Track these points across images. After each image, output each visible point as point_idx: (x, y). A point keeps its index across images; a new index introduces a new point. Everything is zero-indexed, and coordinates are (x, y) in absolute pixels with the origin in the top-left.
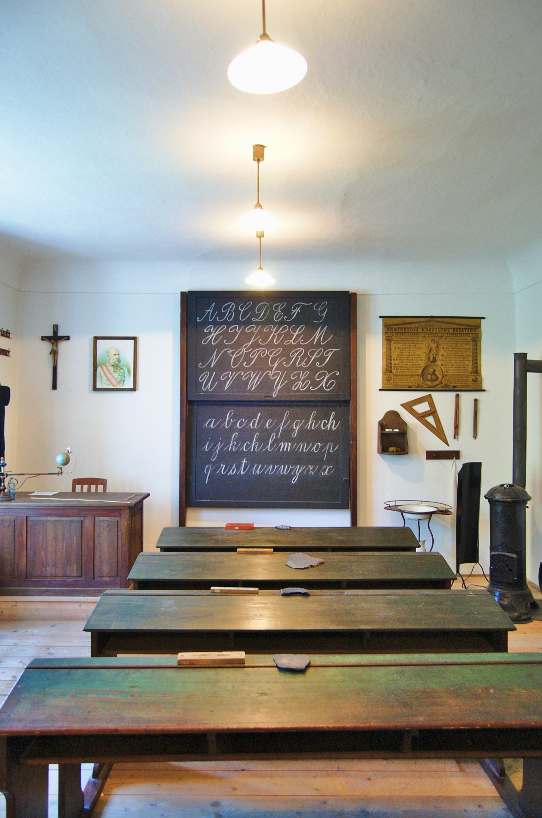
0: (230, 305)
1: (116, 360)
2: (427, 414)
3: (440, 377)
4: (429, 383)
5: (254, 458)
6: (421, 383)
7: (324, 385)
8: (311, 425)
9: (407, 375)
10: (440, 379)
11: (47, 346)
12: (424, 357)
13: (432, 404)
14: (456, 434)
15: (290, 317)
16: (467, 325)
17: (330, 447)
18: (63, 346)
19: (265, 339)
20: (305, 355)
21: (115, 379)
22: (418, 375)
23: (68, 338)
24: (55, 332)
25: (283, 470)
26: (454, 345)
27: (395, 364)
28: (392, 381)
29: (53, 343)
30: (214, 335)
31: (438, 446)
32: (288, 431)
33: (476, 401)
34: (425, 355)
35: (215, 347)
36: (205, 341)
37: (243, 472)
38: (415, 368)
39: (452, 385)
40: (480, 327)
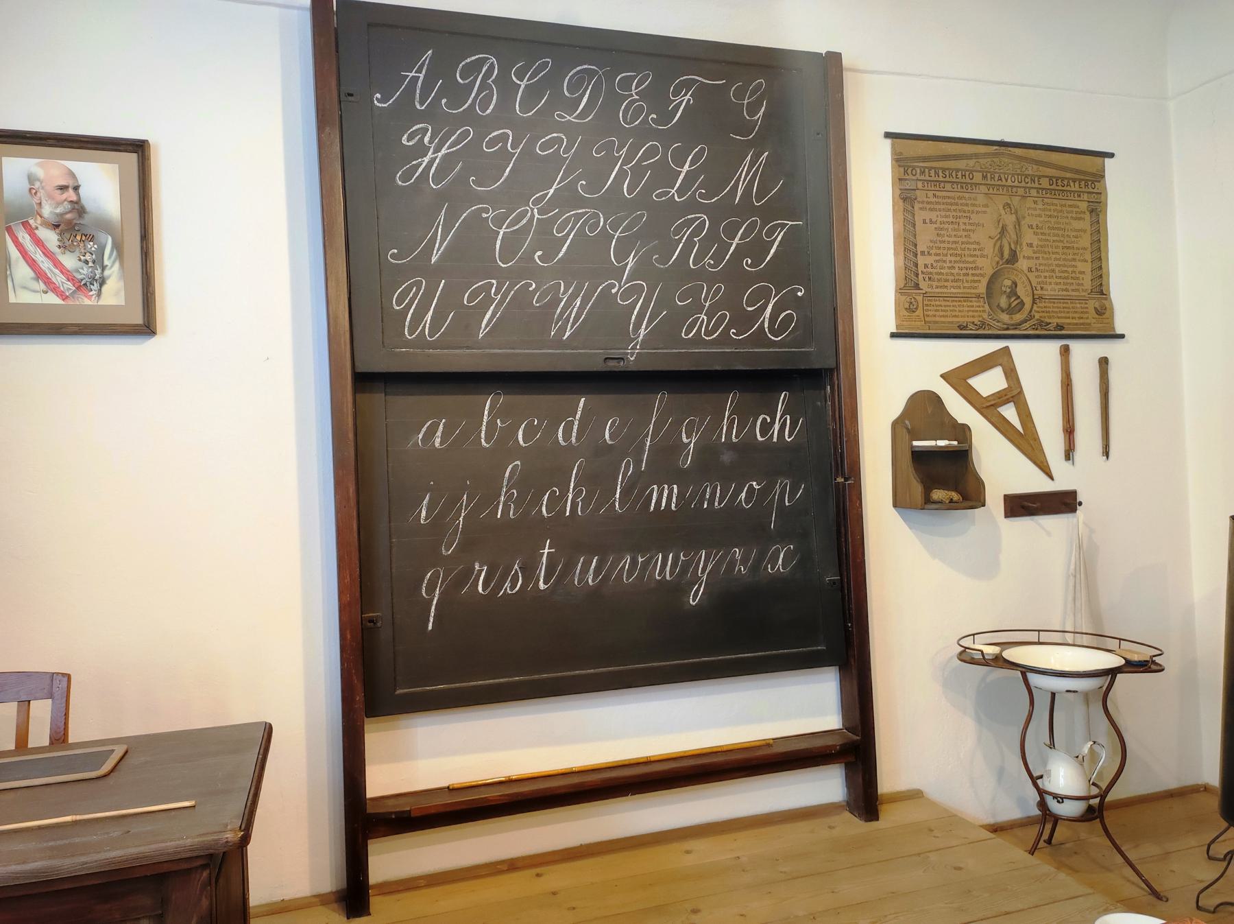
0: (481, 62)
1: (67, 206)
2: (1002, 398)
3: (1028, 301)
4: (1005, 317)
5: (576, 539)
6: (985, 316)
7: (766, 325)
8: (729, 431)
9: (953, 297)
10: (1027, 306)
12: (989, 248)
13: (1011, 373)
14: (1069, 454)
15: (666, 116)
16: (1077, 172)
17: (786, 494)
19: (596, 181)
20: (713, 236)
21: (63, 270)
22: (978, 297)
25: (663, 567)
26: (1053, 220)
27: (926, 266)
28: (919, 312)
30: (432, 159)
31: (1031, 481)
32: (668, 450)
33: (1104, 362)
34: (992, 242)
35: (441, 197)
36: (405, 178)
37: (545, 583)
38: (970, 278)
39: (1055, 321)
40: (1103, 177)
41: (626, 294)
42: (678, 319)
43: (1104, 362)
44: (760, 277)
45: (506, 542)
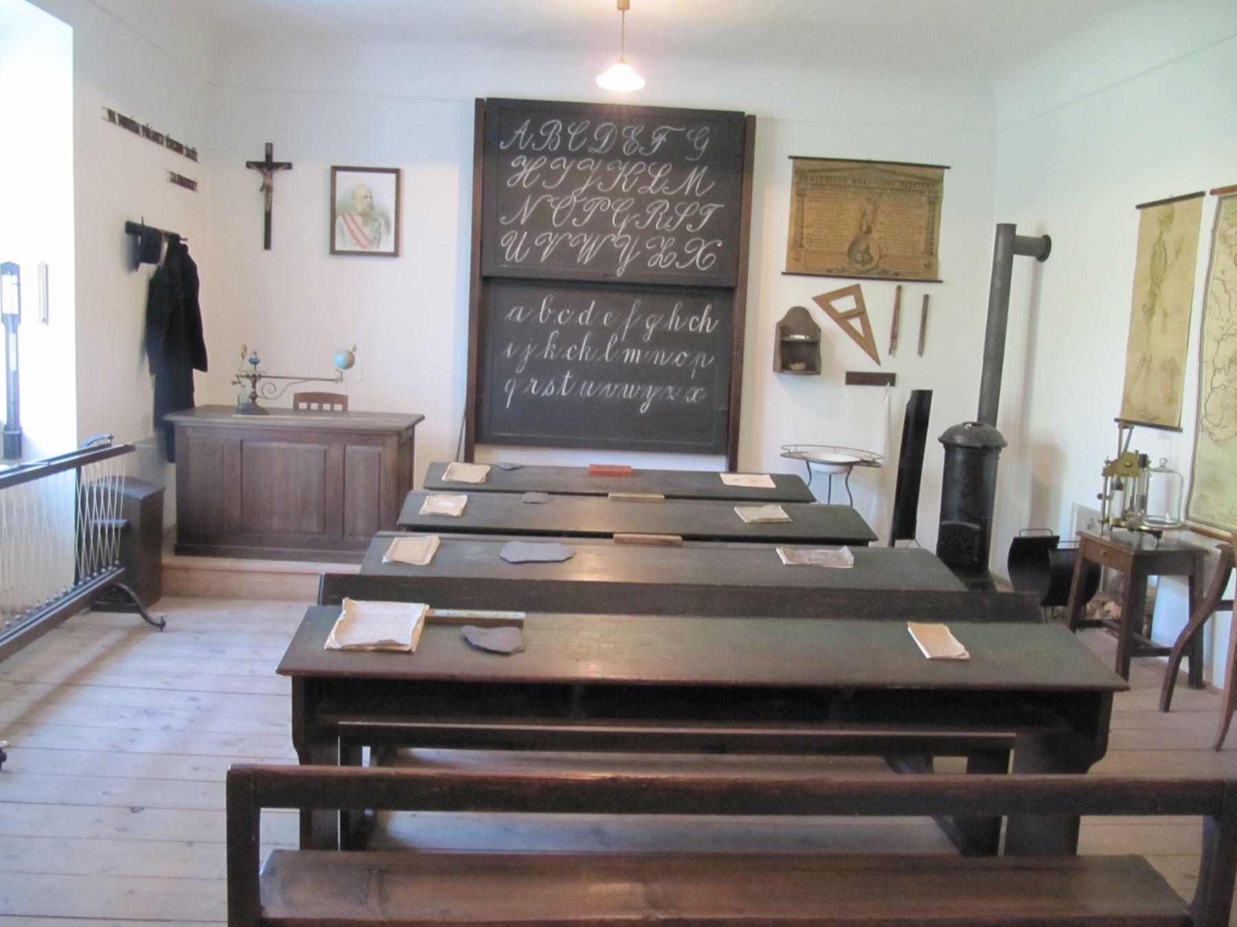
4: (859, 267)
5: (583, 372)
10: (875, 261)
11: (256, 177)
13: (859, 300)
14: (893, 348)
16: (921, 178)
17: (702, 360)
18: (279, 177)
23: (289, 166)
24: (269, 156)
25: (628, 391)
28: (802, 261)
29: (265, 174)
30: (525, 173)
31: (865, 365)
33: (926, 297)
41: (618, 243)
42: (647, 255)
43: (926, 297)
44: (696, 234)
45: (546, 370)
